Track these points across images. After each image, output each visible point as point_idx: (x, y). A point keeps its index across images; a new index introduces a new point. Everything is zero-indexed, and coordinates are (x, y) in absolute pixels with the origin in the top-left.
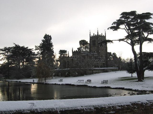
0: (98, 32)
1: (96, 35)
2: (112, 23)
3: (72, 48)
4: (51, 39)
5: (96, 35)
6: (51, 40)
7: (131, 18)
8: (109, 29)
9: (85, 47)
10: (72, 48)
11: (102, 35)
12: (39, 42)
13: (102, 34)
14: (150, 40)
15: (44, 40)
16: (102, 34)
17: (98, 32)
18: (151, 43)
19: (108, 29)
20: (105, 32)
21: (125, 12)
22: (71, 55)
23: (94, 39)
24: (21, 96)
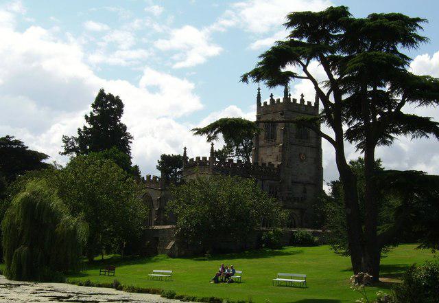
0: (259, 93)
1: (309, 103)
2: (259, 55)
3: (185, 149)
4: (120, 111)
5: (265, 103)
6: (120, 116)
7: (336, 37)
8: (250, 79)
9: (245, 148)
10: (185, 149)
11: (302, 100)
12: (75, 122)
13: (302, 96)
14: (422, 126)
15: (96, 114)
16: (302, 96)
17: (259, 93)
18: (424, 137)
19: (245, 79)
20: (259, 89)
21: (296, 11)
22: (159, 174)
23: (269, 117)
24: (384, 273)
